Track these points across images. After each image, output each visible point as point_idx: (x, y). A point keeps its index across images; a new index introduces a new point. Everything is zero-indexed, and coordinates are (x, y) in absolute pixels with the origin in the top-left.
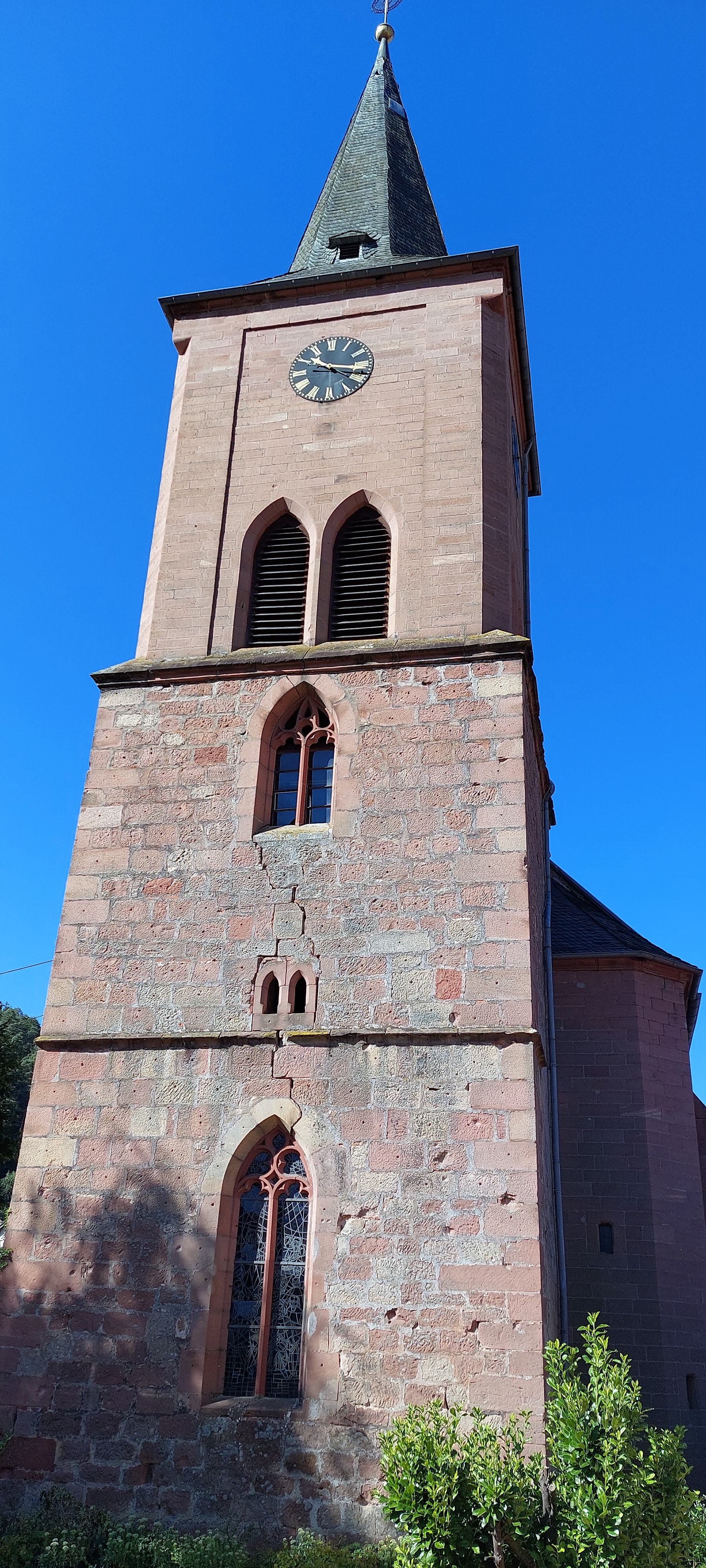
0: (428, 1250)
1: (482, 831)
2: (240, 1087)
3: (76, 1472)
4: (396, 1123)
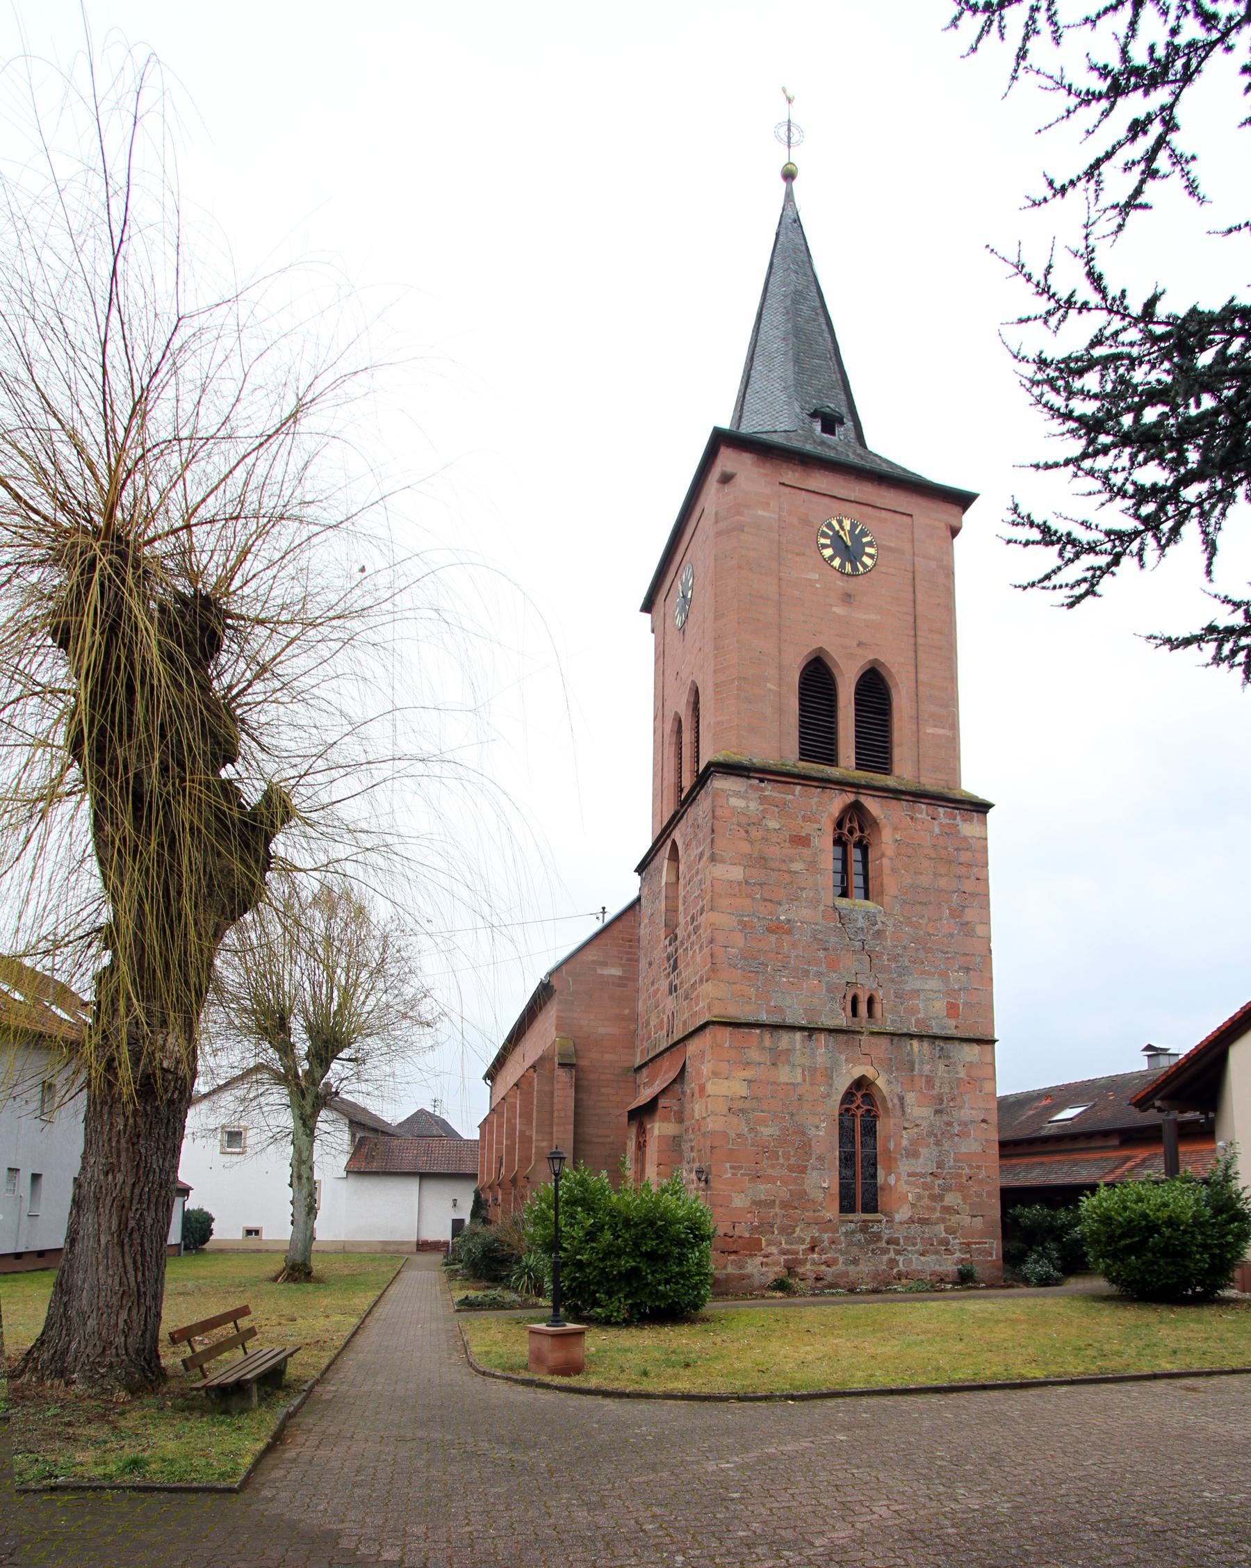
0: (946, 1146)
1: (968, 923)
2: (843, 1057)
3: (775, 1251)
4: (930, 1081)
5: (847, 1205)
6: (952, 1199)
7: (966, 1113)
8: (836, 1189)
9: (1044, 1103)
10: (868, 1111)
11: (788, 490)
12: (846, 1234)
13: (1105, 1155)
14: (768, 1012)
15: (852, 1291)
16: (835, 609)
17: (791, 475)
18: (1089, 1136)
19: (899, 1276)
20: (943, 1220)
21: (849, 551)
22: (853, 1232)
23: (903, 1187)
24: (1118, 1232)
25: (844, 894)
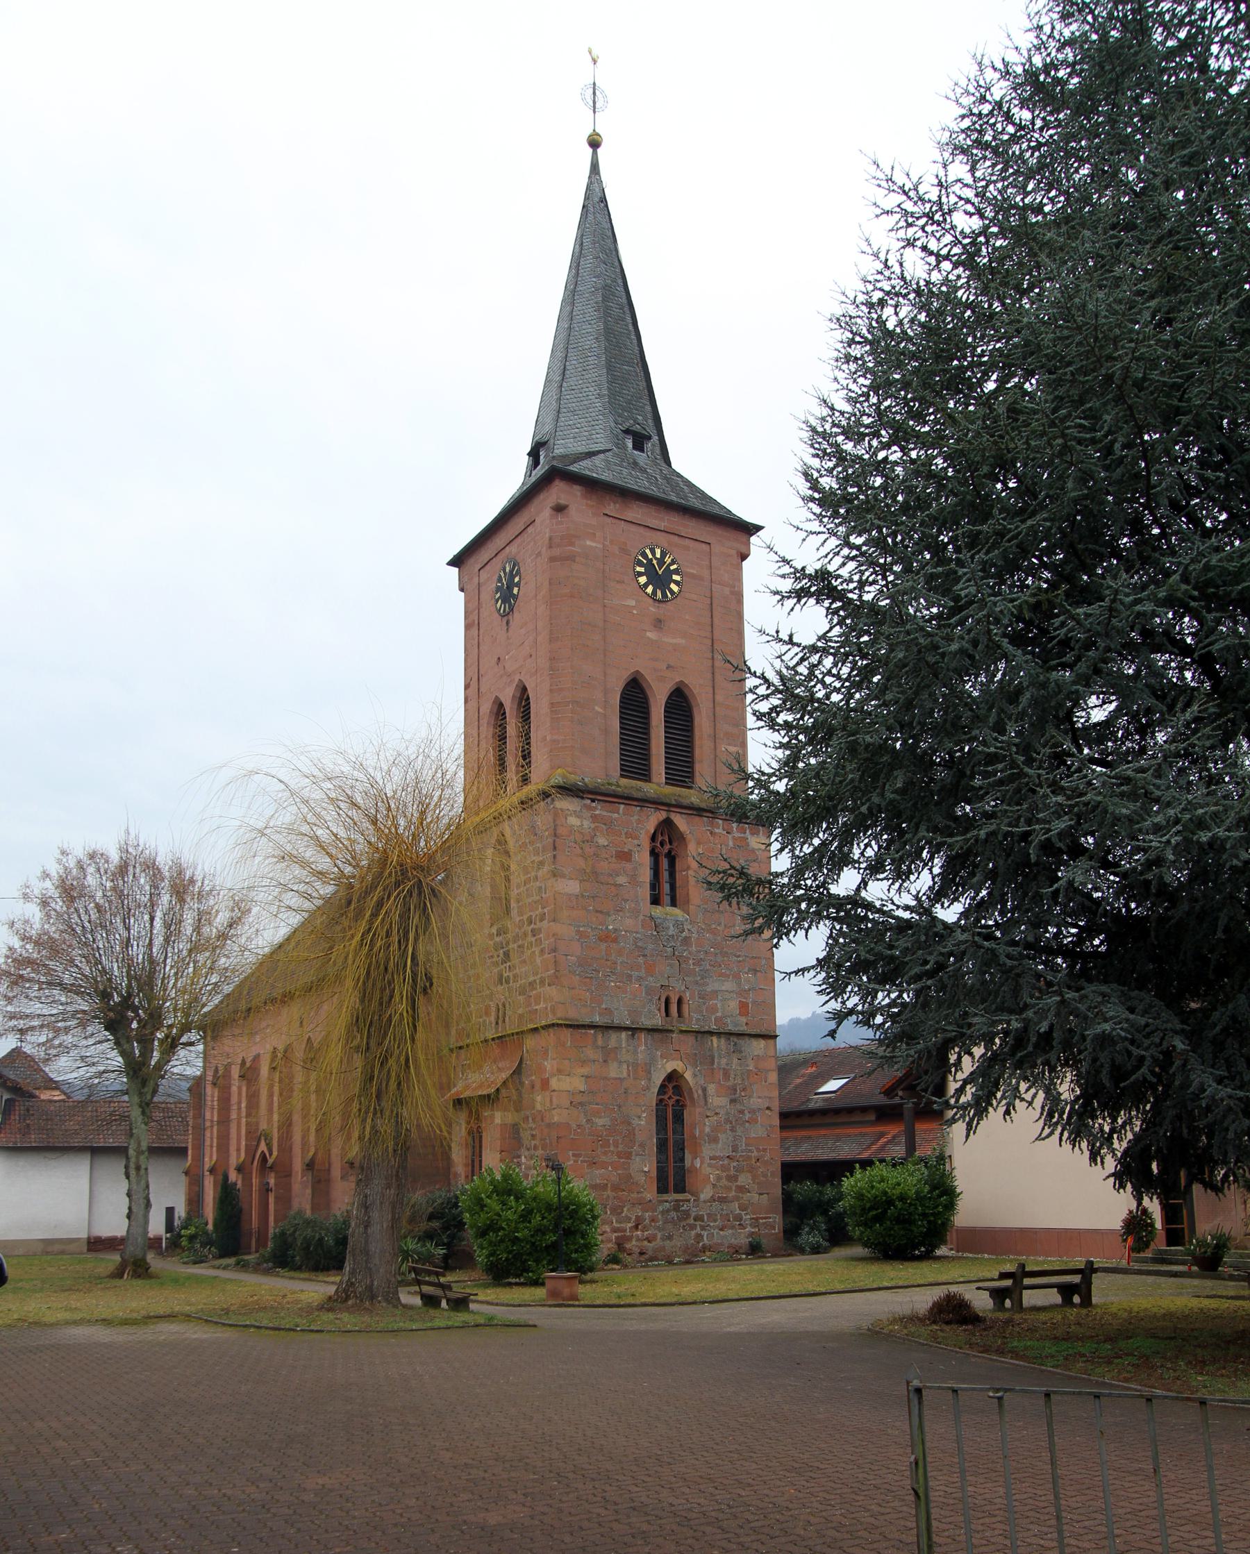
4: (726, 1074)
5: (662, 1189)
6: (744, 1179)
7: (755, 1102)
8: (654, 1174)
9: (810, 1070)
10: (678, 1101)
11: (609, 520)
12: (663, 1213)
13: (864, 1130)
14: (600, 1015)
15: (670, 1262)
16: (649, 634)
17: (612, 508)
18: (850, 1111)
19: (704, 1249)
20: (737, 1198)
21: (660, 580)
22: (668, 1211)
23: (706, 1170)
24: (868, 1205)
25: (655, 901)
